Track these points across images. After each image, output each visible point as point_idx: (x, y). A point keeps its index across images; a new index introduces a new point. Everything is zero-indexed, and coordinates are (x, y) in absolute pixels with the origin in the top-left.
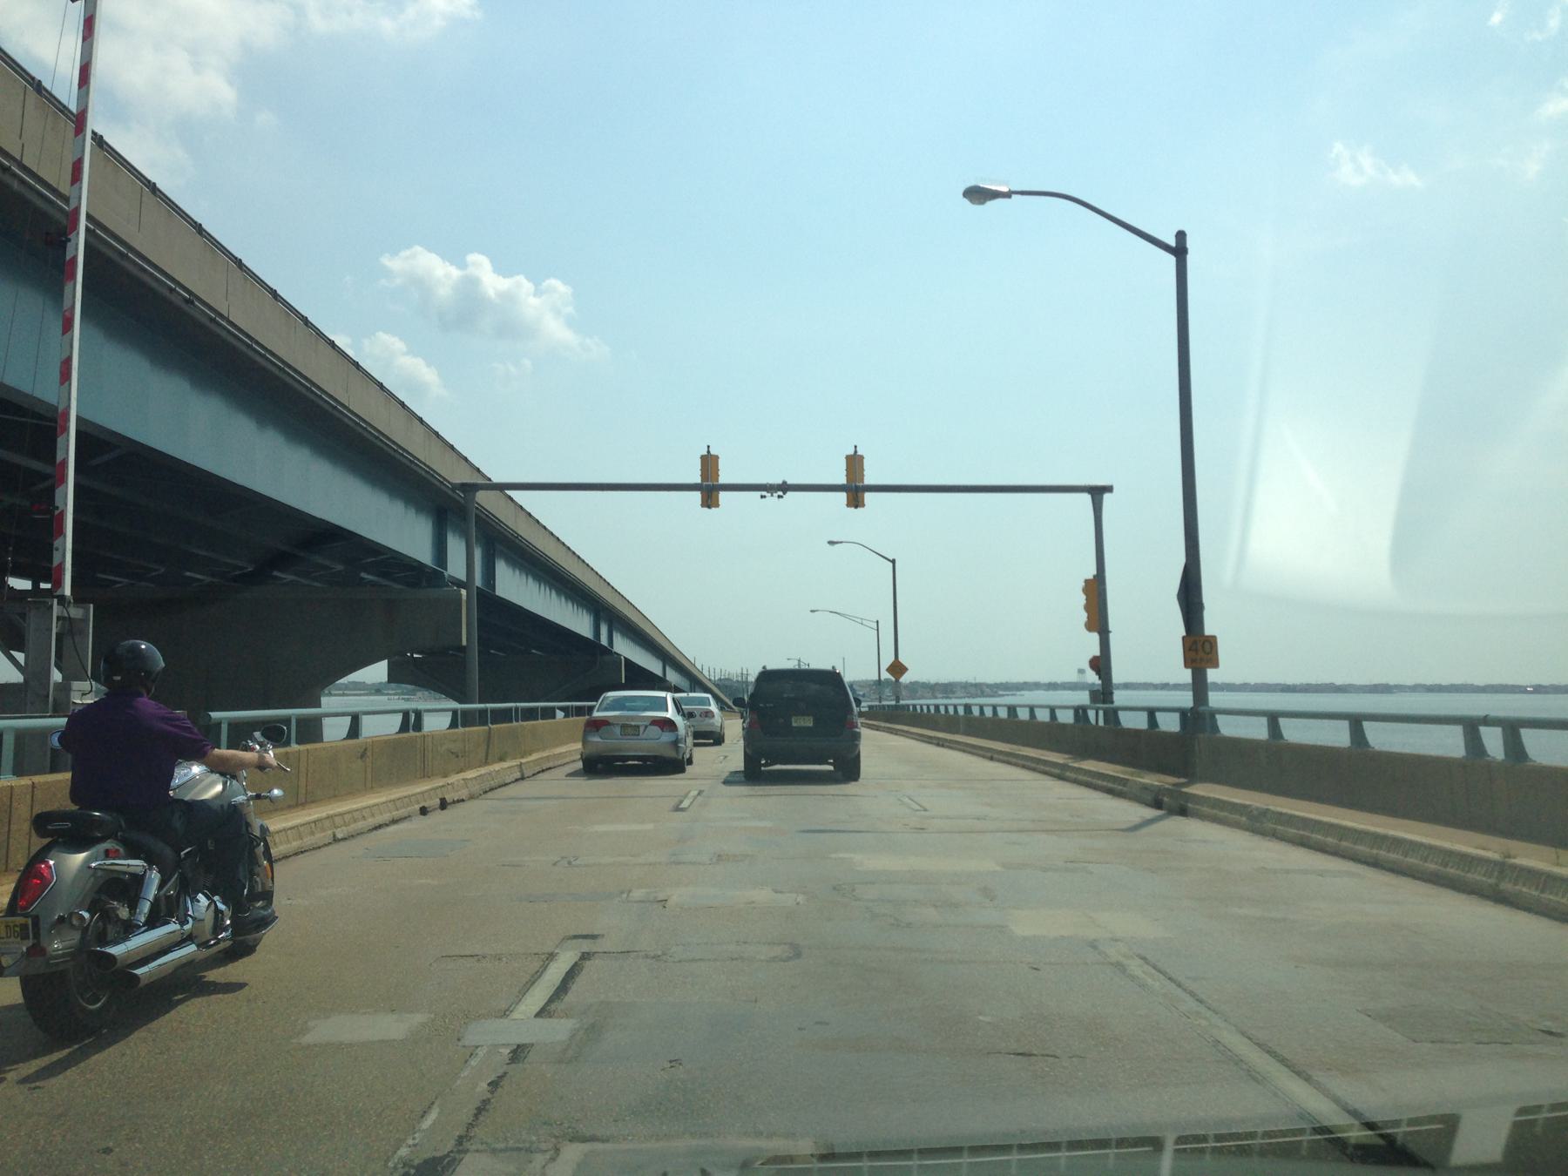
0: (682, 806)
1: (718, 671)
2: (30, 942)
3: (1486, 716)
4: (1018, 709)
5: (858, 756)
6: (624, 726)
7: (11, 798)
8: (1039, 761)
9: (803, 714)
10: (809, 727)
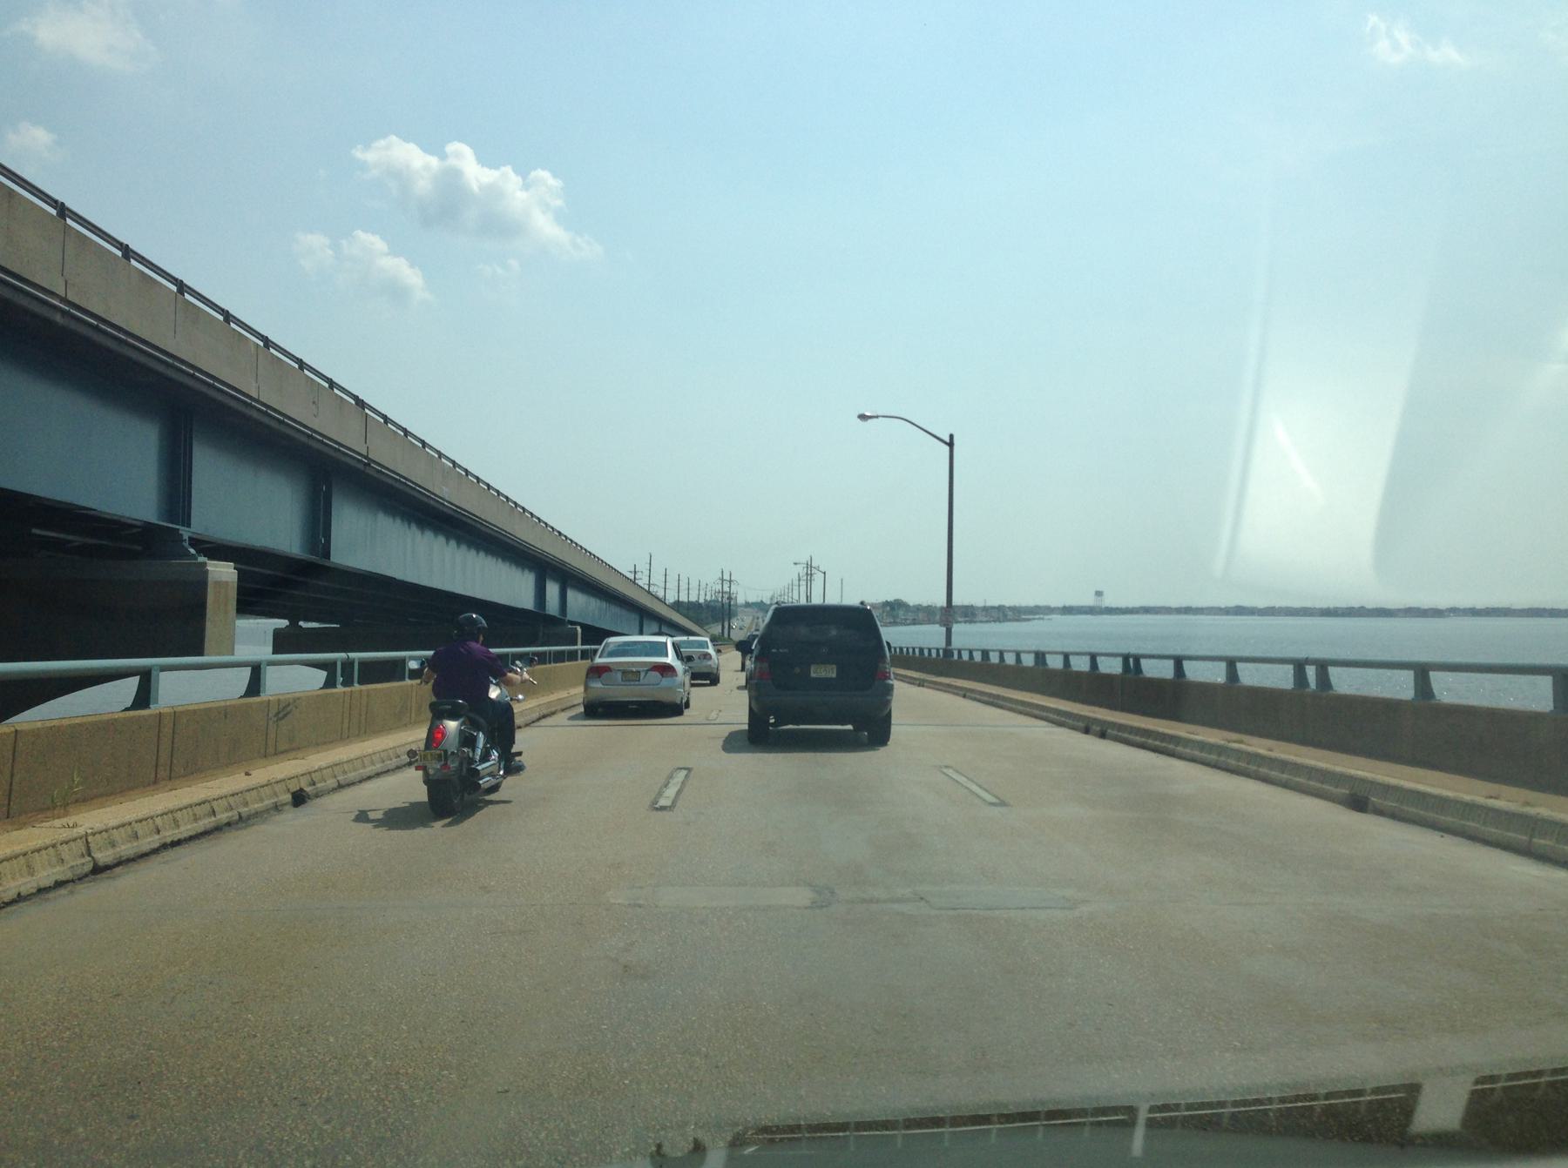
0: (663, 802)
1: (694, 584)
2: (443, 763)
3: (1307, 658)
4: (1047, 656)
5: (889, 716)
6: (624, 672)
7: (14, 752)
8: (1023, 703)
9: (824, 662)
10: (831, 679)
